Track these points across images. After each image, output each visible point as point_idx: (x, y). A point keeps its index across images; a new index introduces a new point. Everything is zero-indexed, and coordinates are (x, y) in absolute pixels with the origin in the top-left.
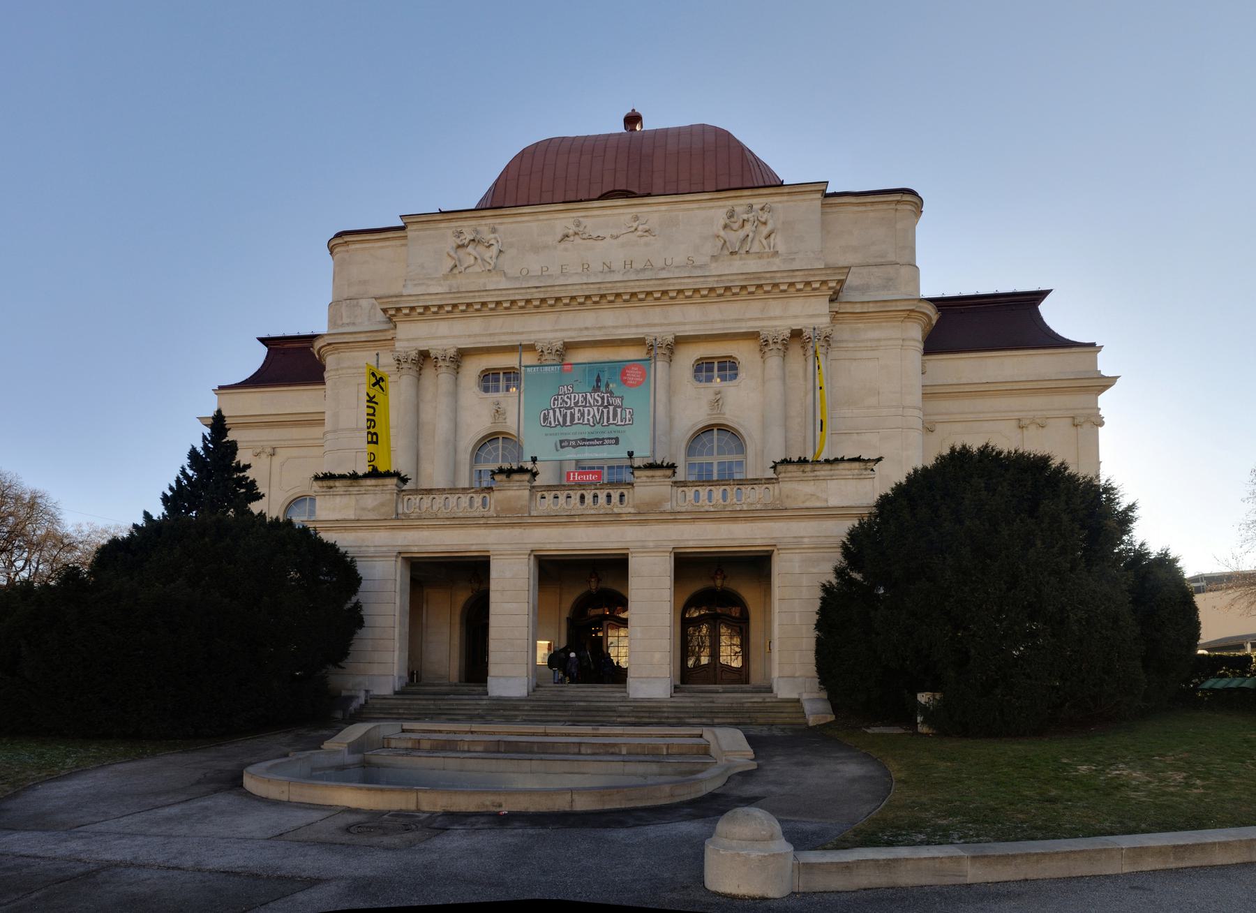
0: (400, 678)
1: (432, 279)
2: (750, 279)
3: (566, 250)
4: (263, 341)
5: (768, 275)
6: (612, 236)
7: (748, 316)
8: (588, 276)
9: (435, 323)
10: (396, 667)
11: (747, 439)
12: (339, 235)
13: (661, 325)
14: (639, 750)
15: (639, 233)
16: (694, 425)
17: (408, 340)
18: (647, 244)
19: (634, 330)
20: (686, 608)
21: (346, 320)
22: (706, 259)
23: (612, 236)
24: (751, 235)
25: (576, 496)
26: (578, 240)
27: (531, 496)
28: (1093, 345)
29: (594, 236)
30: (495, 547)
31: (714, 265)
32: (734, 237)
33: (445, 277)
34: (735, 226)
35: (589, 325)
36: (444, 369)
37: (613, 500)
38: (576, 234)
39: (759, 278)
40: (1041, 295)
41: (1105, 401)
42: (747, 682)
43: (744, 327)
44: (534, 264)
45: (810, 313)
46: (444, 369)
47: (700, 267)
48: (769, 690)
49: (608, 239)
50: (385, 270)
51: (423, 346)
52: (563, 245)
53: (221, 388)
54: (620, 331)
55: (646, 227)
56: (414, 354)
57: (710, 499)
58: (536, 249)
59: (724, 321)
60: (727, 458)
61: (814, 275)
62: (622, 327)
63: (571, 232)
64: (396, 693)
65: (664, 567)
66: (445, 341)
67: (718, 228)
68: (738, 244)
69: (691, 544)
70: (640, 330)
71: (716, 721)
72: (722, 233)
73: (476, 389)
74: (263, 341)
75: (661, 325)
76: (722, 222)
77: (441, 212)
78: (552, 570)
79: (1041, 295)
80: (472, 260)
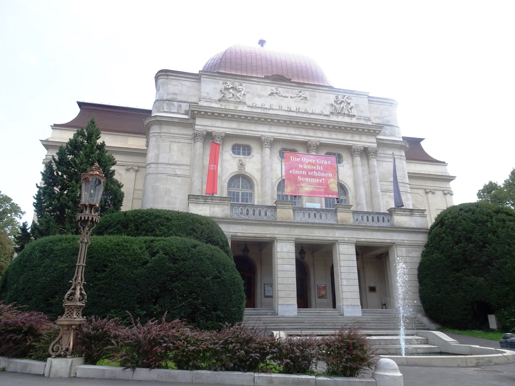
3: (272, 98)
4: (80, 104)
6: (291, 97)
7: (347, 139)
11: (348, 190)
12: (160, 71)
13: (314, 137)
14: (414, 352)
17: (201, 126)
21: (166, 110)
22: (328, 113)
23: (291, 97)
24: (345, 107)
26: (277, 96)
28: (444, 163)
29: (284, 95)
33: (220, 100)
34: (338, 102)
37: (375, 220)
38: (276, 93)
39: (352, 125)
40: (422, 139)
41: (452, 185)
43: (345, 143)
44: (259, 102)
45: (369, 142)
47: (327, 115)
48: (343, 315)
50: (175, 87)
51: (210, 129)
53: (55, 125)
56: (362, 148)
57: (266, 215)
58: (259, 96)
60: (246, 191)
62: (298, 135)
63: (274, 92)
65: (352, 250)
66: (219, 129)
72: (334, 104)
73: (231, 152)
74: (80, 104)
75: (314, 137)
78: (363, 251)
79: (422, 139)
80: (231, 96)
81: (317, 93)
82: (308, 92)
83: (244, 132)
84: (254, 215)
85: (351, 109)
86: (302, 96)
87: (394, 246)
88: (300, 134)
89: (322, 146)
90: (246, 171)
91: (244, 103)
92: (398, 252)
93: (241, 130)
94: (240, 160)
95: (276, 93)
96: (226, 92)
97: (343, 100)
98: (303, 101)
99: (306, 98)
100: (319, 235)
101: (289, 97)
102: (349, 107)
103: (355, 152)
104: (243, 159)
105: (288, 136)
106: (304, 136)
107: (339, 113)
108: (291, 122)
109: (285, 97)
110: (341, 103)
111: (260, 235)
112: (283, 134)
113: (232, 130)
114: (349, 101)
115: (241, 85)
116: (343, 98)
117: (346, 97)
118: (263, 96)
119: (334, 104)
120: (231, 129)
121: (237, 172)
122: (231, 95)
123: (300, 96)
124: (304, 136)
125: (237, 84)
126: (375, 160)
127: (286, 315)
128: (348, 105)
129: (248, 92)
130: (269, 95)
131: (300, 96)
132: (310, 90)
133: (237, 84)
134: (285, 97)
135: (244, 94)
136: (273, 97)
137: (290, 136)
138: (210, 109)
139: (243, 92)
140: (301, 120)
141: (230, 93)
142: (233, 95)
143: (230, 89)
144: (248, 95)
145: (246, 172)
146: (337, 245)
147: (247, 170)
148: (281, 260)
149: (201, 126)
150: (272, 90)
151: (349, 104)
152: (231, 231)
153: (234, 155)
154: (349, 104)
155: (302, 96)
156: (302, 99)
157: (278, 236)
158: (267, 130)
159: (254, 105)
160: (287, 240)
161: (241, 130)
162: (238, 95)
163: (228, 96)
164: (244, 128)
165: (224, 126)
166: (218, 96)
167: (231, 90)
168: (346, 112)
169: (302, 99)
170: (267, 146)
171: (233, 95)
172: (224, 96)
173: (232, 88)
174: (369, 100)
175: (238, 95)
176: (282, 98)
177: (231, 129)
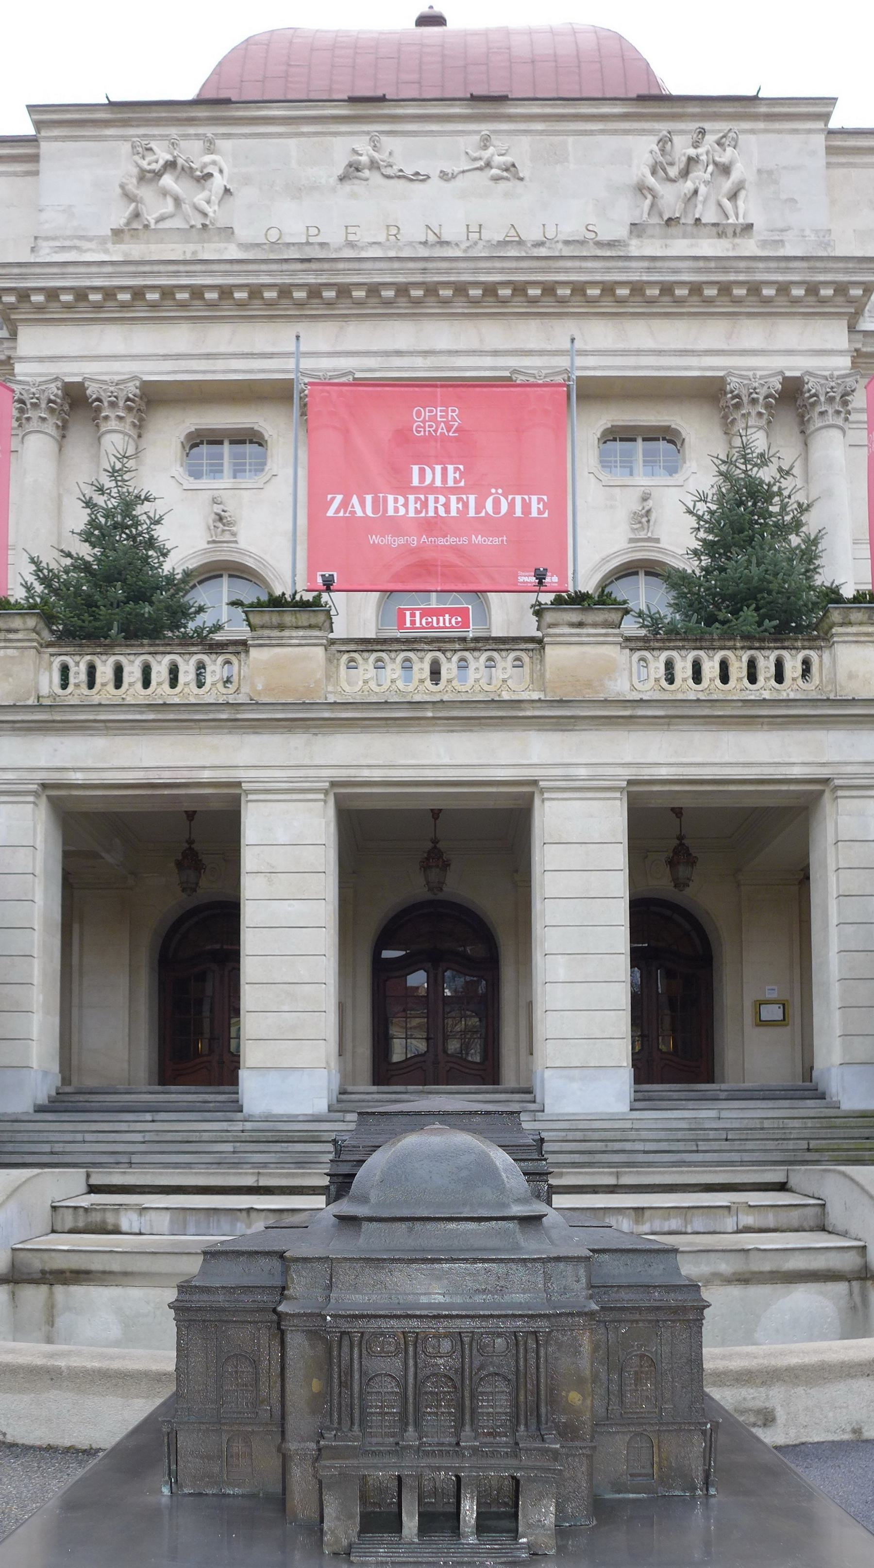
0: (45, 1073)
1: (89, 239)
2: (708, 271)
3: (353, 195)
5: (742, 264)
6: (445, 176)
7: (702, 346)
8: (400, 249)
9: (96, 329)
10: (229, 947)
13: (541, 353)
15: (495, 171)
16: (605, 560)
17: (41, 359)
18: (507, 195)
19: (488, 361)
23: (445, 176)
24: (703, 190)
25: (422, 667)
26: (376, 178)
27: (329, 661)
30: (252, 773)
31: (634, 242)
32: (670, 197)
33: (117, 233)
34: (673, 172)
35: (401, 345)
36: (113, 424)
38: (374, 165)
39: (725, 270)
42: (711, 1080)
46: (113, 424)
48: (839, 1108)
49: (435, 180)
51: (73, 372)
52: (347, 187)
54: (462, 361)
55: (508, 159)
58: (297, 191)
59: (659, 353)
61: (825, 270)
63: (364, 159)
64: (39, 1109)
65: (611, 821)
66: (117, 366)
67: (640, 169)
68: (680, 206)
69: (664, 773)
70: (501, 361)
71: (626, 1180)
72: (651, 181)
73: (178, 470)
75: (541, 353)
76: (648, 159)
77: (112, 104)
80: (169, 206)
81: (571, 139)
82: (525, 140)
83: (220, 364)
84: (146, 683)
85: (733, 196)
86: (498, 160)
87: (827, 795)
88: (476, 346)
89: (160, 135)
90: (243, 544)
91: (228, 232)
92: (843, 820)
93: (208, 356)
94: (215, 501)
95: (374, 165)
96: (146, 193)
97: (692, 152)
98: (503, 185)
99: (511, 168)
100: (446, 761)
101: (435, 175)
102: (727, 185)
103: (737, 406)
104: (225, 495)
105: (419, 362)
106: (496, 353)
107: (670, 219)
108: (431, 290)
109: (418, 178)
110: (685, 173)
111: (166, 777)
112: (399, 353)
113: (169, 365)
114: (724, 159)
115: (210, 149)
116: (696, 145)
117: (710, 139)
118: (314, 188)
119: (651, 181)
120: (166, 357)
121: (205, 551)
122: (170, 201)
123: (488, 165)
124: (496, 353)
125: (191, 151)
126: (836, 434)
127: (280, 1108)
128: (721, 179)
129: (247, 181)
130: (342, 179)
131: (488, 165)
132: (539, 126)
133: (191, 151)
134: (418, 178)
135: (227, 191)
136: (356, 187)
137: (430, 361)
138: (63, 276)
139: (218, 182)
140: (476, 271)
141: (165, 193)
142: (177, 201)
143: (158, 175)
144: (244, 195)
145: (240, 551)
146: (537, 802)
147: (243, 543)
148: (260, 878)
149: (41, 359)
150: (355, 152)
151: (725, 170)
152: (43, 764)
153: (191, 483)
154: (725, 170)
155: (498, 160)
156: (496, 179)
157: (252, 773)
158: (324, 347)
159: (273, 236)
160: (295, 791)
161: (208, 356)
162: (200, 199)
163: (154, 208)
164: (223, 349)
165: (135, 351)
166: (119, 216)
167: (167, 180)
168: (710, 216)
169: (496, 179)
170: (831, 419)
171: (177, 201)
172: (137, 215)
173: (171, 165)
174: (830, 150)
175: (200, 199)
176: (401, 184)
177: (166, 357)
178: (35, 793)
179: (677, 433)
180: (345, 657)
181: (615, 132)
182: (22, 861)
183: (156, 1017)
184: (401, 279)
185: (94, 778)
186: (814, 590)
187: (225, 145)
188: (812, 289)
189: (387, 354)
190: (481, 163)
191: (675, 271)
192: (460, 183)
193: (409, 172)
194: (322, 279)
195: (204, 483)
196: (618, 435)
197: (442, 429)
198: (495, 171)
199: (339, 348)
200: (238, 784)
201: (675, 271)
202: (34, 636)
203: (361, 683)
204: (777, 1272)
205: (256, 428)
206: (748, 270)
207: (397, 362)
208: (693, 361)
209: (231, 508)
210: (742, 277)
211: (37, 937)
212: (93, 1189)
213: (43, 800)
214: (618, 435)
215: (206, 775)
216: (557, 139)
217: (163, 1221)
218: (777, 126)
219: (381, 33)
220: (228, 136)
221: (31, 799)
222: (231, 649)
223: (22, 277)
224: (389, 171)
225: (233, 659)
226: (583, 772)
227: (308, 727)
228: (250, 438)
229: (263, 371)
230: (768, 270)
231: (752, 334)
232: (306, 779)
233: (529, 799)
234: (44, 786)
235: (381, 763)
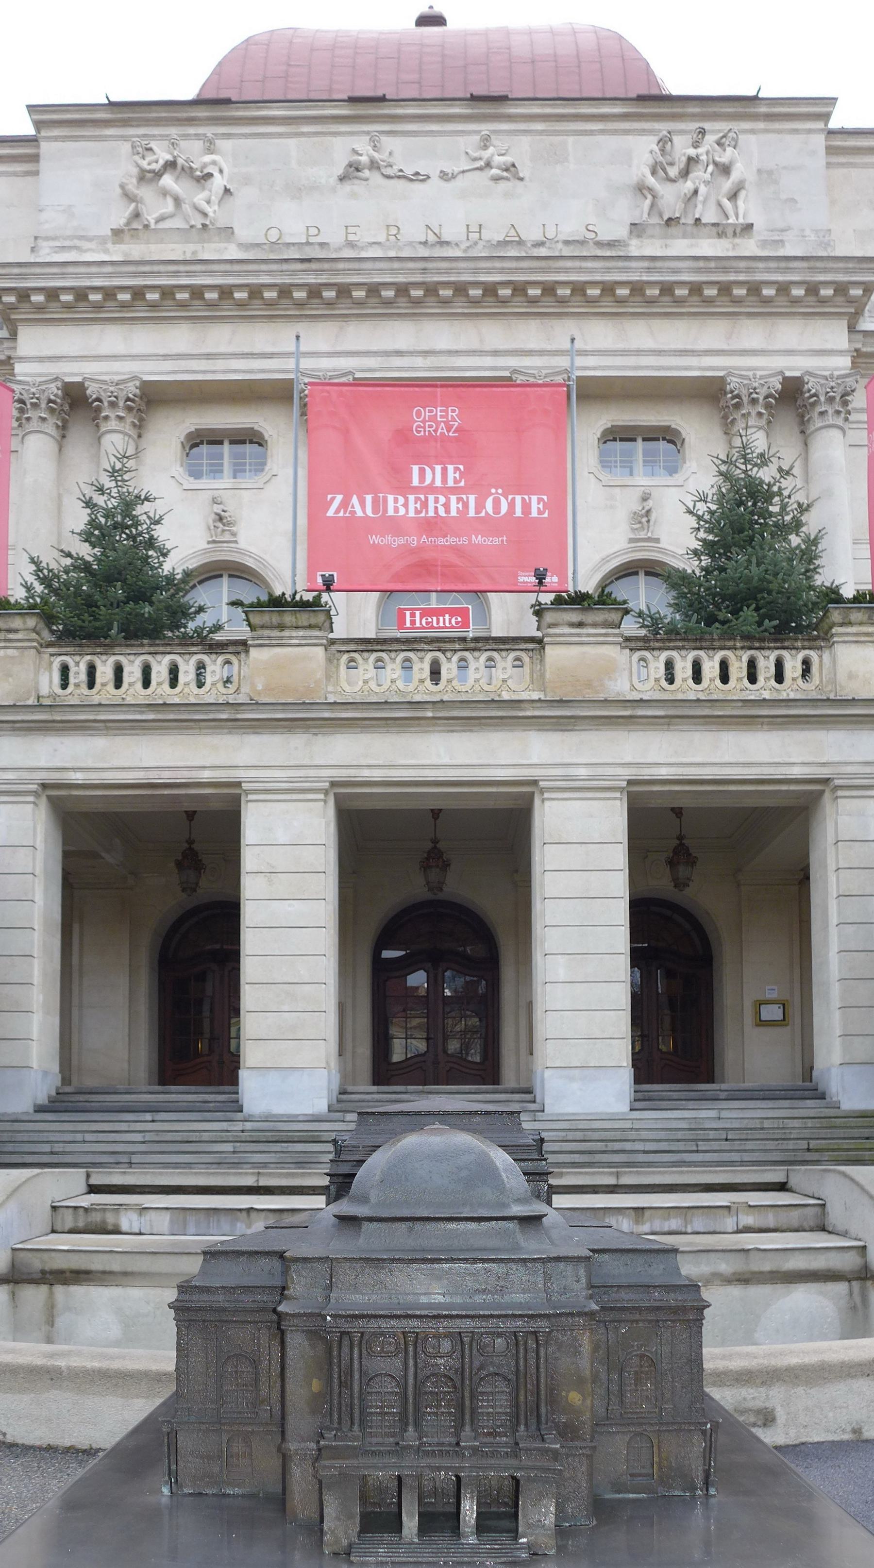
0: (45, 1073)
1: (89, 239)
2: (708, 271)
3: (353, 195)
5: (742, 264)
6: (445, 176)
7: (702, 346)
8: (400, 249)
9: (96, 329)
13: (541, 353)
15: (495, 171)
16: (605, 560)
17: (41, 359)
18: (507, 195)
19: (488, 361)
20: (384, 940)
23: (445, 176)
24: (703, 190)
25: (422, 667)
26: (376, 178)
27: (329, 661)
30: (252, 773)
31: (634, 242)
32: (670, 197)
33: (117, 233)
34: (673, 172)
35: (401, 345)
36: (113, 424)
38: (374, 165)
39: (725, 270)
42: (711, 1080)
46: (113, 424)
49: (435, 180)
51: (73, 372)
52: (347, 187)
54: (462, 361)
55: (508, 159)
58: (297, 191)
59: (659, 353)
61: (825, 270)
63: (364, 159)
64: (39, 1109)
65: (611, 821)
66: (117, 366)
67: (640, 169)
68: (680, 206)
69: (664, 773)
70: (501, 361)
72: (651, 181)
73: (178, 470)
75: (541, 353)
76: (648, 159)
77: (112, 104)
80: (169, 206)
81: (571, 139)
82: (525, 140)
83: (220, 364)
84: (146, 683)
85: (733, 196)
86: (498, 160)
87: (827, 795)
88: (476, 346)
90: (243, 544)
91: (228, 232)
92: (843, 820)
93: (208, 356)
94: (215, 501)
95: (374, 165)
96: (146, 193)
97: (692, 152)
98: (503, 185)
99: (511, 168)
100: (446, 761)
101: (435, 175)
102: (727, 185)
103: (737, 406)
104: (225, 495)
105: (419, 362)
106: (496, 353)
107: (670, 219)
108: (431, 290)
109: (418, 178)
110: (685, 173)
111: (166, 777)
112: (399, 353)
113: (169, 365)
114: (724, 159)
115: (210, 149)
116: (696, 145)
117: (710, 139)
118: (314, 188)
119: (651, 181)
120: (166, 357)
121: (205, 551)
122: (170, 201)
123: (488, 165)
124: (496, 353)
125: (191, 151)
126: (836, 434)
127: (280, 1108)
128: (721, 179)
129: (247, 181)
130: (342, 179)
131: (488, 165)
132: (539, 126)
133: (191, 151)
134: (418, 178)
135: (227, 191)
136: (356, 187)
137: (430, 361)
138: (63, 276)
139: (218, 182)
140: (476, 271)
141: (165, 193)
142: (177, 201)
143: (158, 175)
144: (244, 195)
145: (240, 551)
146: (537, 802)
147: (243, 543)
148: (260, 878)
149: (41, 359)
150: (355, 152)
151: (725, 170)
152: (43, 764)
153: (191, 483)
154: (725, 170)
155: (498, 160)
156: (496, 179)
157: (252, 773)
158: (324, 347)
159: (273, 236)
160: (295, 791)
161: (208, 356)
162: (200, 199)
163: (154, 208)
164: (223, 349)
165: (135, 351)
166: (119, 216)
167: (167, 180)
168: (710, 216)
169: (496, 179)
170: (831, 419)
171: (177, 201)
172: (137, 215)
173: (171, 165)
174: (830, 150)
175: (200, 199)
176: (401, 184)
177: (166, 357)
178: (35, 793)
179: (677, 433)
180: (345, 657)
181: (615, 132)
182: (22, 861)
183: (156, 1017)
184: (401, 279)
185: (94, 778)
186: (814, 590)
187: (225, 145)
188: (812, 289)
189: (387, 354)
190: (481, 163)
191: (675, 271)
192: (460, 183)
193: (409, 172)
194: (322, 279)
195: (204, 483)
196: (618, 435)
197: (442, 429)
198: (495, 171)
199: (339, 348)
200: (238, 784)
201: (675, 271)
202: (34, 636)
203: (361, 683)
204: (777, 1272)
205: (256, 428)
206: (748, 270)
207: (397, 362)
208: (693, 361)
209: (231, 508)
210: (742, 277)
211: (37, 937)
212: (93, 1189)
213: (43, 800)
214: (618, 435)
215: (206, 775)
216: (557, 139)
217: (163, 1221)
218: (777, 126)
219: (381, 33)
220: (228, 136)
221: (31, 799)
222: (231, 649)
223: (22, 277)
224: (389, 171)
225: (233, 659)
226: (583, 772)
227: (308, 727)
228: (250, 438)
229: (263, 371)
230: (768, 270)
231: (752, 334)
232: (306, 779)
233: (529, 799)
234: (44, 786)
235: (381, 763)
